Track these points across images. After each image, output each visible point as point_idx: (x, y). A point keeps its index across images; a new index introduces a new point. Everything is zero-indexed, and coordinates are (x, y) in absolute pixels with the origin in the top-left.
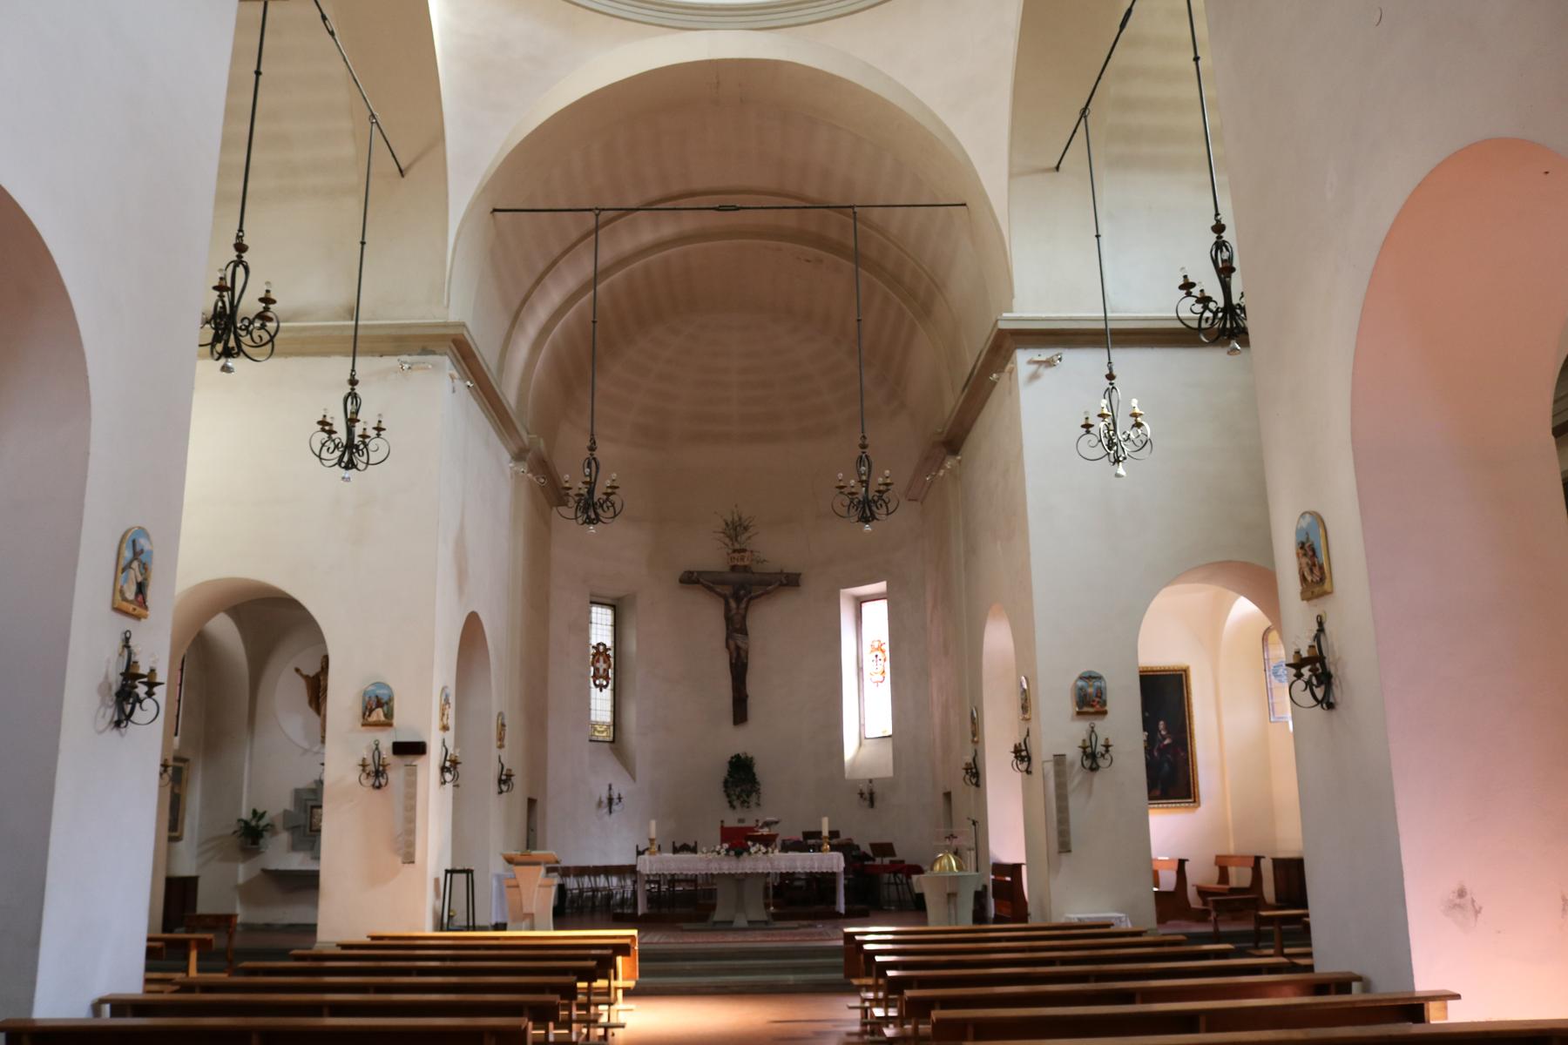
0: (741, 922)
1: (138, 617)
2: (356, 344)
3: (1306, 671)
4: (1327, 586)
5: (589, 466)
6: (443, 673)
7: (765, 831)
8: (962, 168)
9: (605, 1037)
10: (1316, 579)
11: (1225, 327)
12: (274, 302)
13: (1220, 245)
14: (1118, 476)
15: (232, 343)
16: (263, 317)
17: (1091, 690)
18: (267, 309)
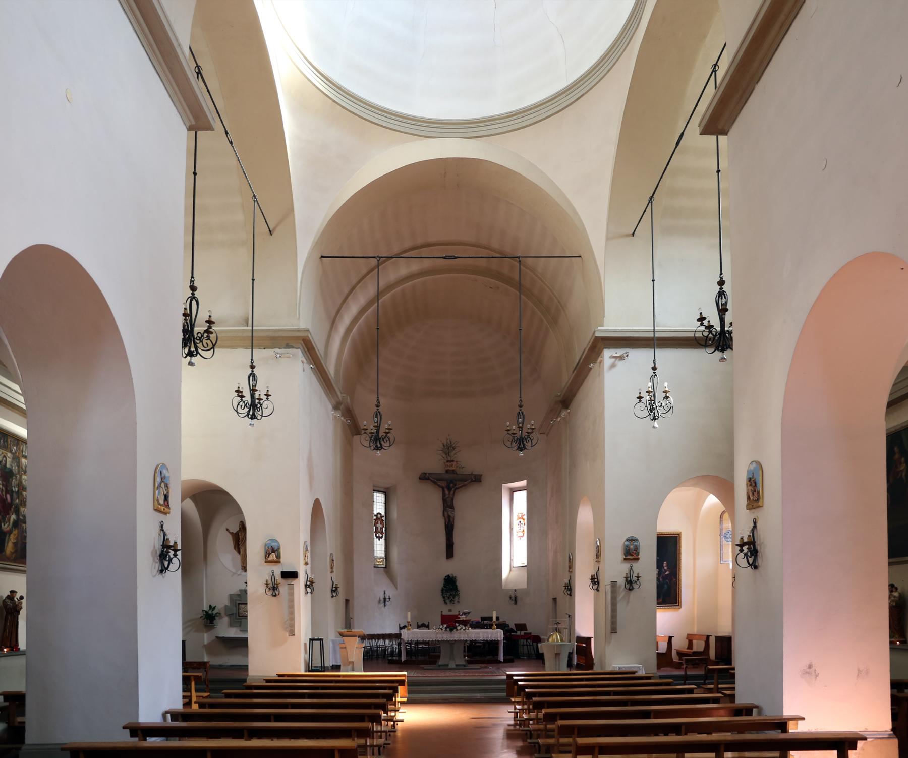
0: (452, 665)
1: (166, 514)
2: (253, 341)
3: (745, 548)
4: (760, 503)
5: (376, 416)
6: (304, 535)
7: (463, 618)
9: (394, 725)
10: (755, 499)
11: (720, 341)
12: (214, 323)
13: (721, 294)
14: (654, 427)
15: (193, 349)
17: (632, 547)
18: (210, 327)
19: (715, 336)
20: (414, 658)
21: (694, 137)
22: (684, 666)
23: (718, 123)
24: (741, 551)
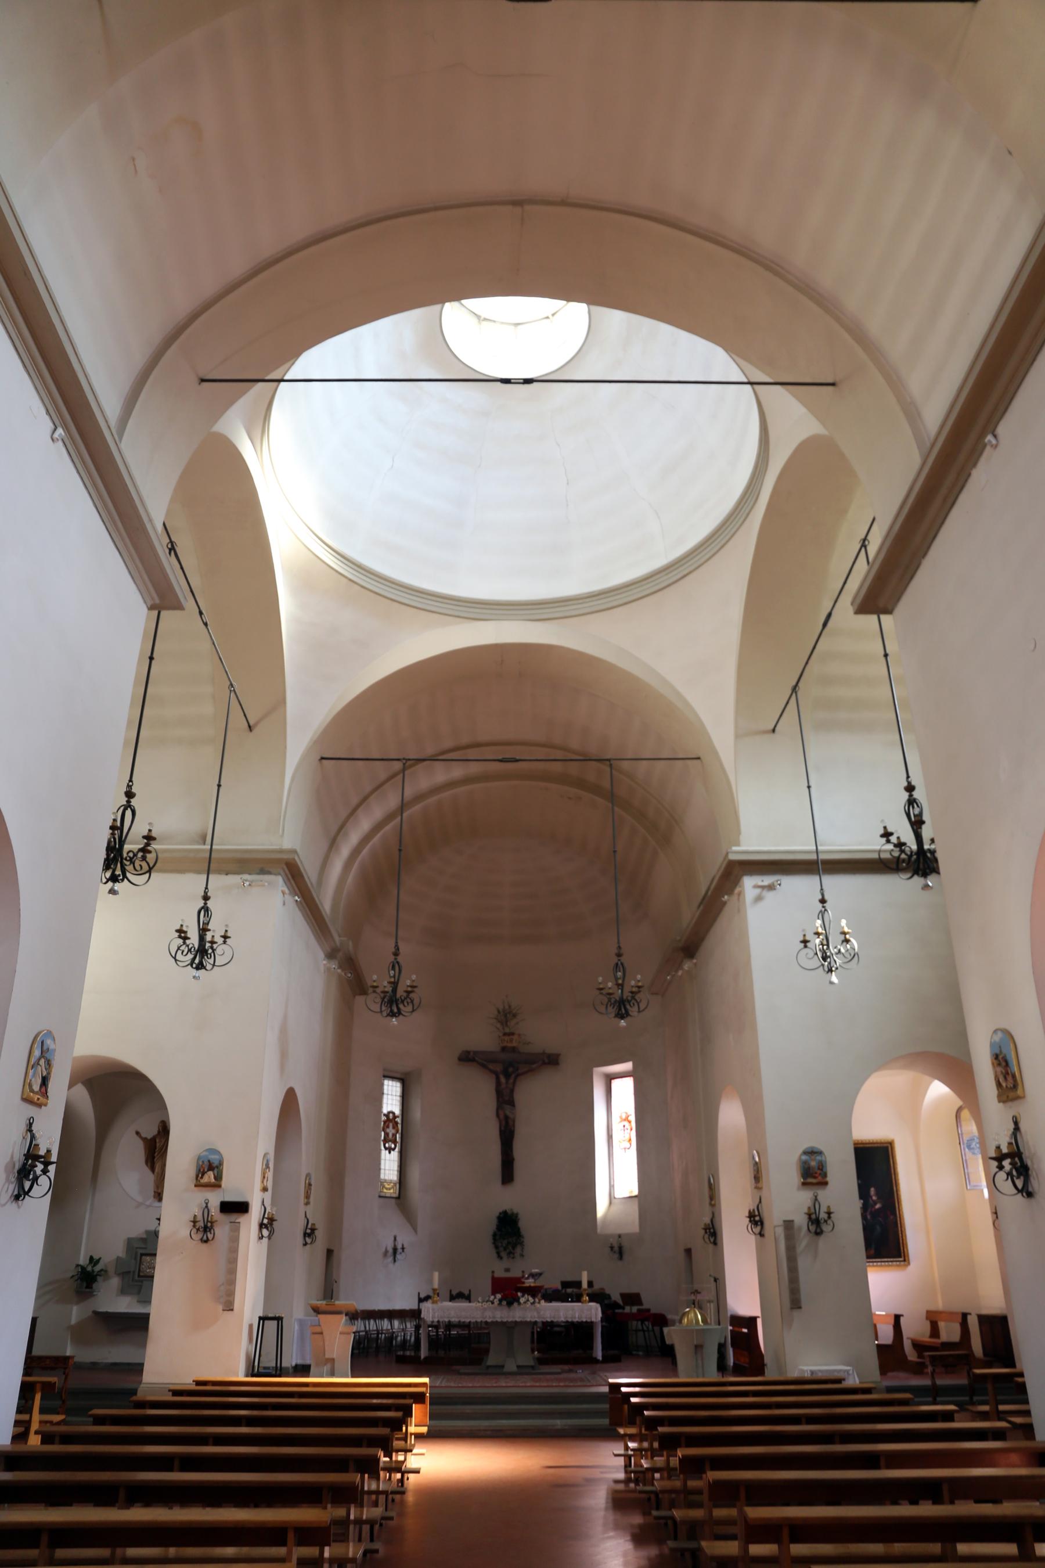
0: (511, 1366)
1: (40, 1105)
2: (211, 864)
3: (1006, 1163)
4: (1019, 1092)
5: (393, 968)
6: (265, 1143)
7: (530, 1282)
8: (699, 730)
9: (402, 1481)
11: (921, 863)
13: (911, 802)
14: (831, 983)
15: (118, 872)
16: (144, 850)
17: (813, 1164)
18: (147, 844)
19: (910, 856)
20: (441, 1353)
21: (845, 614)
22: (930, 1369)
23: (879, 597)
24: (1001, 1167)
